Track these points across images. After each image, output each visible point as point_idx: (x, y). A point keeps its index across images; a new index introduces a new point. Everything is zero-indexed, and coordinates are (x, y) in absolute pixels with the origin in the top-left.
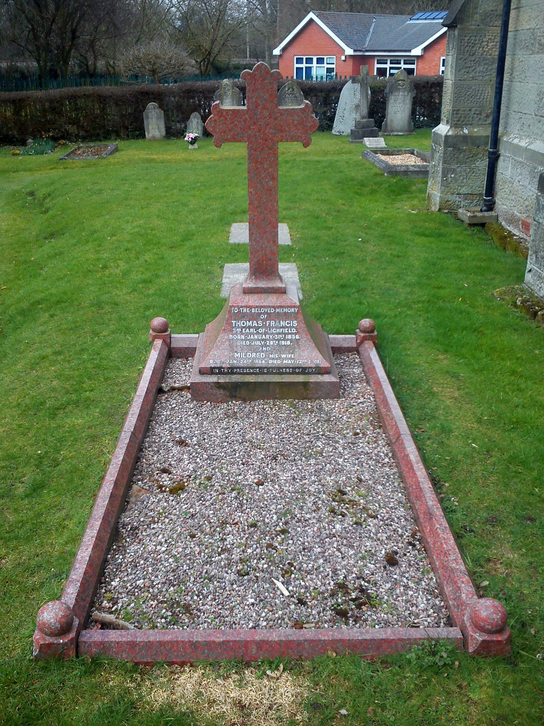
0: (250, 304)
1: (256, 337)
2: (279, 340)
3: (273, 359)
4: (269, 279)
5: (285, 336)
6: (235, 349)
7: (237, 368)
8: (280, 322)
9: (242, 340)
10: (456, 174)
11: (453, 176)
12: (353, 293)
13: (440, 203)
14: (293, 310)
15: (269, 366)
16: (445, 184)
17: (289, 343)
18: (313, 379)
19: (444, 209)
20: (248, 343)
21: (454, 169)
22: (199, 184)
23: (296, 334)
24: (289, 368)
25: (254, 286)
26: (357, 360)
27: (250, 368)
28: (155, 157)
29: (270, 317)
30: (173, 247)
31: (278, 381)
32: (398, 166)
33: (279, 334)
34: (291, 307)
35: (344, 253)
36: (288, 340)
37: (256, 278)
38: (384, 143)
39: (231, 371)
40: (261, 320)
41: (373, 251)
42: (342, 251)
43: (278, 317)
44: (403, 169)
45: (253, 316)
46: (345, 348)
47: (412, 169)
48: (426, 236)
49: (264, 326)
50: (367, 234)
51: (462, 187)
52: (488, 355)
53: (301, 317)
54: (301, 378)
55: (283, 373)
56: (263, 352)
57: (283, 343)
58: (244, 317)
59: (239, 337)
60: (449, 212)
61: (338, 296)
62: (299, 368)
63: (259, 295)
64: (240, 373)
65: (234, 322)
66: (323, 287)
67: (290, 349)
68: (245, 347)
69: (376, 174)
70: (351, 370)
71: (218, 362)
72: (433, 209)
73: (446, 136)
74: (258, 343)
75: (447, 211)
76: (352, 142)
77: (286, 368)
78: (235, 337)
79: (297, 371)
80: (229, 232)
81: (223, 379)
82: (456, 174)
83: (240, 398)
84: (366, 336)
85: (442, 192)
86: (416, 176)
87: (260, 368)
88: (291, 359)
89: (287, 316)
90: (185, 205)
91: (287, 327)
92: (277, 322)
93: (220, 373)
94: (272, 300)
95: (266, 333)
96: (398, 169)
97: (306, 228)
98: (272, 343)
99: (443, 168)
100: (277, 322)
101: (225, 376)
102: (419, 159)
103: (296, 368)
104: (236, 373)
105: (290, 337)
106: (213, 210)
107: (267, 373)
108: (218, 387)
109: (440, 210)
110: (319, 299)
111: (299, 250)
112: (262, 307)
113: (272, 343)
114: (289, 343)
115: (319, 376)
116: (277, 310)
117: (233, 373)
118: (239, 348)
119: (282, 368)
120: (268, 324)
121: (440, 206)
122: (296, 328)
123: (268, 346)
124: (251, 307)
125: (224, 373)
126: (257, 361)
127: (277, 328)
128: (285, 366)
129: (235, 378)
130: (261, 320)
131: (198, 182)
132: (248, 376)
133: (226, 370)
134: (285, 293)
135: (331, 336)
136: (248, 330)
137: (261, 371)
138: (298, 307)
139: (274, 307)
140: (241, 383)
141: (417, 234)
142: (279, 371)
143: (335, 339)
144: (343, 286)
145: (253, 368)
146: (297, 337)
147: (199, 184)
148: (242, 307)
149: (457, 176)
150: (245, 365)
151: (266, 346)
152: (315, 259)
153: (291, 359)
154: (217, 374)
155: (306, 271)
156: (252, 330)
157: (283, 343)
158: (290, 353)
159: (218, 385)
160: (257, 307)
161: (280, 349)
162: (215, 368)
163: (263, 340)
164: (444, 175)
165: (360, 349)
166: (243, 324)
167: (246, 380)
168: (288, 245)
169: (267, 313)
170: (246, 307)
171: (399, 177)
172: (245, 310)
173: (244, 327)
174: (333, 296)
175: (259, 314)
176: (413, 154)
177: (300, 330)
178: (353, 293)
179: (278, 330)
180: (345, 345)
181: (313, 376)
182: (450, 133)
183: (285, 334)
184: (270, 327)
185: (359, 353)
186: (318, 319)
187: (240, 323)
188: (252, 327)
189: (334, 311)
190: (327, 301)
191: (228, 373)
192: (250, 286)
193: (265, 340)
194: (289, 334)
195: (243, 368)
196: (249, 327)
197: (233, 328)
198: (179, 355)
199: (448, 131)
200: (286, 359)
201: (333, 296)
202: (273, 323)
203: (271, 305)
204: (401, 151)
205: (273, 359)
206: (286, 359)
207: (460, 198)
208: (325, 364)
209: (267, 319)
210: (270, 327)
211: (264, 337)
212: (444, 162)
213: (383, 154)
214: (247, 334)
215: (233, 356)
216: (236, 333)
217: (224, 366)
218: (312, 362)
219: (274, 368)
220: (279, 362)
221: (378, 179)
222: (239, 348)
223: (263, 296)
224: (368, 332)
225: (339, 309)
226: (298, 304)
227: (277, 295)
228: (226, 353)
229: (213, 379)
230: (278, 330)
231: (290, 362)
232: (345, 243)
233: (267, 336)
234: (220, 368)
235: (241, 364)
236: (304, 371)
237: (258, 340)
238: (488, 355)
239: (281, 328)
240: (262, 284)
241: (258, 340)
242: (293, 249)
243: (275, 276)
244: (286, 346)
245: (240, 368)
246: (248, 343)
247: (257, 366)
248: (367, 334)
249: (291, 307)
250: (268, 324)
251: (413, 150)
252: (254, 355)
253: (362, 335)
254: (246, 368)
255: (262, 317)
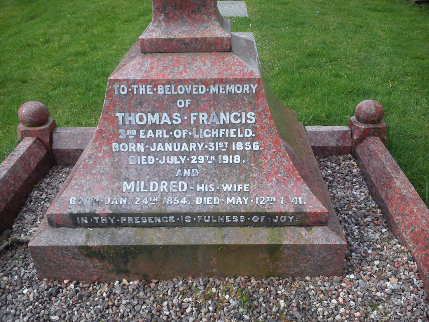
0: (153, 75)
1: (169, 147)
2: (216, 154)
3: (204, 194)
4: (195, 21)
5: (230, 145)
6: (125, 173)
7: (126, 215)
8: (218, 116)
9: (139, 154)
12: (325, 63)
14: (246, 88)
15: (196, 210)
17: (237, 159)
18: (291, 237)
20: (152, 160)
23: (252, 140)
24: (239, 214)
25: (164, 36)
26: (355, 171)
27: (154, 215)
29: (197, 103)
30: (126, 21)
31: (214, 242)
33: (216, 140)
34: (241, 81)
35: (304, 23)
36: (236, 152)
37: (169, 18)
39: (116, 220)
40: (179, 110)
41: (333, 22)
42: (302, 21)
43: (215, 103)
45: (161, 102)
46: (333, 148)
48: (379, 11)
49: (185, 124)
50: (323, 8)
53: (264, 104)
54: (262, 236)
55: (224, 225)
56: (183, 178)
57: (226, 159)
58: (141, 104)
59: (132, 148)
61: (306, 67)
62: (259, 214)
63: (175, 56)
64: (134, 225)
65: (120, 115)
66: (286, 57)
67: (241, 173)
68: (147, 169)
70: (348, 192)
71: (88, 200)
74: (173, 160)
77: (232, 214)
78: (124, 148)
79: (255, 219)
81: (97, 239)
83: (136, 274)
84: (369, 129)
87: (176, 215)
88: (242, 193)
89: (233, 102)
91: (234, 126)
92: (213, 114)
93: (92, 225)
94: (205, 66)
95: (189, 140)
97: (263, 4)
98: (202, 159)
100: (213, 114)
101: (102, 230)
103: (252, 214)
104: (126, 225)
105: (239, 146)
107: (194, 224)
108: (87, 256)
110: (284, 71)
111: (257, 21)
112: (179, 82)
113: (202, 159)
114: (237, 159)
115: (303, 231)
116: (213, 89)
117: (118, 225)
118: (132, 170)
119: (223, 215)
120: (193, 119)
122: (254, 128)
123: (195, 166)
124: (155, 83)
125: (100, 225)
126: (169, 200)
127: (213, 127)
128: (228, 209)
129: (125, 236)
130: (179, 110)
132: (150, 231)
133: (103, 220)
134: (230, 50)
135: (309, 128)
136: (150, 133)
137: (180, 220)
138: (258, 81)
139: (206, 83)
140: (135, 247)
141: (369, 9)
142: (216, 219)
143: (316, 133)
144: (311, 55)
145: (160, 215)
146: (256, 147)
148: (135, 82)
150: (145, 209)
151: (189, 166)
152: (274, 29)
153: (242, 193)
154: (86, 226)
155: (264, 40)
156: (159, 133)
157: (226, 159)
158: (239, 182)
159: (88, 252)
160: (169, 82)
161: (219, 172)
162: (80, 215)
163: (182, 153)
165: (358, 151)
166: (141, 119)
167: (147, 241)
168: (245, 17)
169: (191, 96)
170: (145, 82)
172: (142, 90)
173: (142, 127)
174: (301, 67)
175: (174, 99)
177: (263, 133)
178: (325, 63)
179: (215, 133)
180: (332, 143)
181: (288, 230)
183: (230, 140)
184: (198, 126)
185: (356, 157)
186: (283, 99)
187: (135, 118)
188: (159, 127)
189: (305, 87)
190: (293, 73)
191: (109, 225)
192: (155, 36)
193: (188, 154)
194: (238, 139)
195: (140, 215)
196: (154, 127)
197: (119, 127)
198: (67, 161)
200: (232, 193)
201: (301, 67)
202: (203, 117)
203: (199, 77)
205: (204, 194)
206: (232, 193)
208: (315, 206)
209: (191, 109)
210: (198, 126)
211: (185, 147)
214: (149, 142)
215: (120, 188)
216: (127, 140)
217: (99, 210)
218: (287, 200)
219: (206, 214)
220: (217, 201)
222: (132, 170)
223: (184, 57)
224: (373, 122)
225: (313, 84)
226: (257, 74)
227: (212, 56)
228: (105, 183)
229: (77, 238)
230: (215, 133)
231: (239, 201)
232: (304, 15)
233: (193, 146)
234: (90, 216)
235: (136, 208)
236: (270, 220)
237: (173, 153)
239: (220, 127)
240: (181, 32)
241: (173, 153)
242: (250, 21)
243: (208, 14)
244: (232, 166)
245: (133, 215)
246: (152, 160)
247: (169, 210)
248: (371, 126)
249: (241, 81)
250: (193, 119)
252: (164, 186)
253: (363, 127)
254: (147, 215)
255: (181, 104)
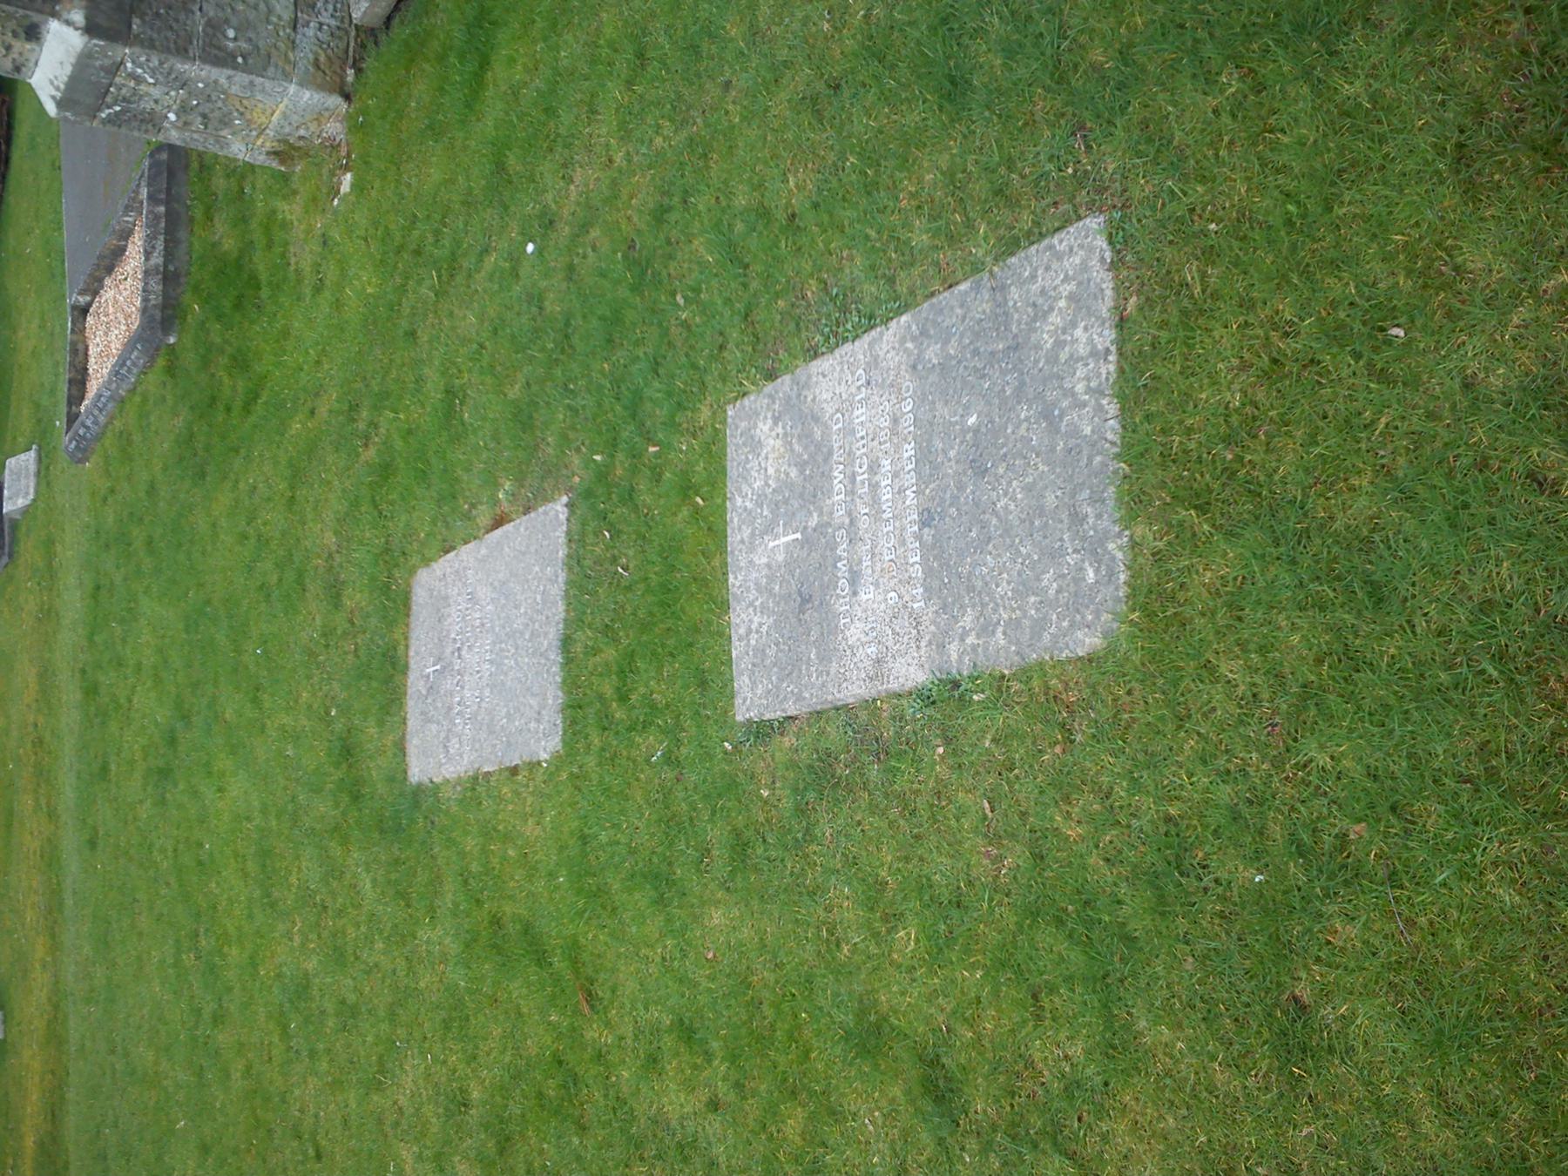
10: (227, 21)
11: (231, 33)
13: (321, 87)
16: (257, 62)
19: (343, 78)
21: (209, 23)
22: (188, 959)
28: (30, 1142)
32: (145, 300)
38: (23, 457)
44: (156, 286)
47: (157, 259)
51: (270, 11)
52: (672, 183)
60: (354, 66)
69: (171, 370)
72: (334, 128)
73: (90, 29)
75: (350, 72)
76: (10, 556)
80: (476, 781)
82: (227, 21)
85: (287, 77)
86: (183, 247)
90: (302, 988)
96: (154, 300)
99: (204, 60)
102: (107, 281)
106: (334, 872)
109: (347, 97)
121: (331, 91)
131: (177, 964)
147: (188, 959)
149: (234, 21)
164: (223, 59)
168: (570, 506)
171: (187, 298)
176: (84, 311)
182: (78, 17)
199: (68, 23)
204: (73, 344)
207: (307, 24)
212: (182, 52)
213: (82, 398)
221: (189, 359)
238: (672, 183)
251: (74, 308)
